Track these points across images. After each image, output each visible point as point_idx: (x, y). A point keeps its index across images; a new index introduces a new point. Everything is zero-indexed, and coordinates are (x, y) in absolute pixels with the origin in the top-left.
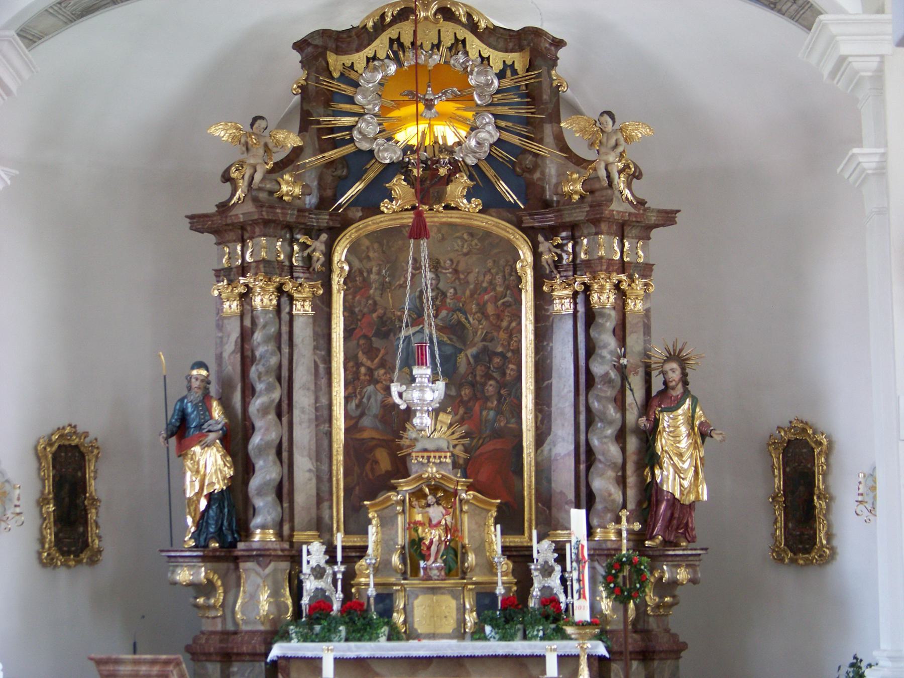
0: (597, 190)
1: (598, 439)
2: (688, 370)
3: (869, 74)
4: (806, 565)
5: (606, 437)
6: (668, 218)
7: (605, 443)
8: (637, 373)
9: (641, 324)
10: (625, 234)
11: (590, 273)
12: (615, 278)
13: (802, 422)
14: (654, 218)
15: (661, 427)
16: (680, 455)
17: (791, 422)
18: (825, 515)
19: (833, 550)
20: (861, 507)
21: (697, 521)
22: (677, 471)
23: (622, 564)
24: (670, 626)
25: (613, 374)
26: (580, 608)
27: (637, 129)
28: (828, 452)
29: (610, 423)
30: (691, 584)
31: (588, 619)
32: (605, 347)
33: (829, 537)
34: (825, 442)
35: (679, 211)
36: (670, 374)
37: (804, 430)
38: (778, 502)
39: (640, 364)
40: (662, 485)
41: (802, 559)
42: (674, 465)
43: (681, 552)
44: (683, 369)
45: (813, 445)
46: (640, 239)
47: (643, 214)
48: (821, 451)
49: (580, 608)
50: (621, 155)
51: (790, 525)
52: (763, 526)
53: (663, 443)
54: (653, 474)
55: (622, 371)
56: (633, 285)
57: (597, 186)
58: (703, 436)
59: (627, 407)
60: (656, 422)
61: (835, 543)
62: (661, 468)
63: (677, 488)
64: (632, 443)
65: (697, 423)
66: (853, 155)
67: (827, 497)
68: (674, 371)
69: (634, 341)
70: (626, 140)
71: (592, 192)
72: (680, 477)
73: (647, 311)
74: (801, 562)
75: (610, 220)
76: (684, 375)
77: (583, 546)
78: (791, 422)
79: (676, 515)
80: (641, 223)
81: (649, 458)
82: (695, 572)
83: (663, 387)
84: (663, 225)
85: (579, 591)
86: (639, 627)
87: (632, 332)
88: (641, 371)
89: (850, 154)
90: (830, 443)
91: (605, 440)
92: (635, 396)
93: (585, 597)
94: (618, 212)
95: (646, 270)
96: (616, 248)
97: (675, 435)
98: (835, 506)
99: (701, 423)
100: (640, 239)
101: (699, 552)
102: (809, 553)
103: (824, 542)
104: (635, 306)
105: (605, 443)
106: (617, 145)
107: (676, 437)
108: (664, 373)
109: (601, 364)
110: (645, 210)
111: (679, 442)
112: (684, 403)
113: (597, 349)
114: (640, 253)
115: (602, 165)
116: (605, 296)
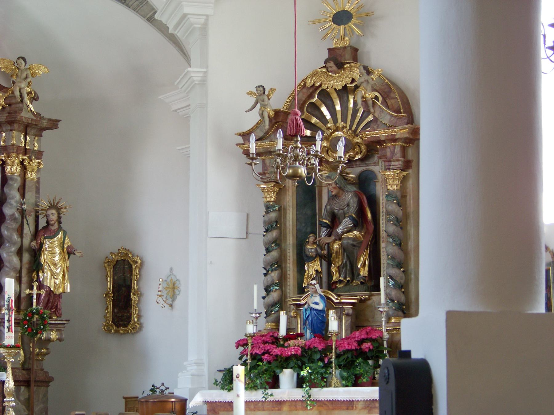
0: (14, 104)
1: (6, 253)
2: (61, 215)
3: (200, 26)
4: (125, 334)
5: (11, 252)
6: (54, 124)
7: (11, 256)
8: (30, 216)
9: (34, 187)
10: (28, 132)
11: (6, 154)
12: (21, 157)
13: (126, 250)
14: (45, 124)
15: (44, 247)
16: (55, 265)
17: (119, 250)
18: (137, 304)
19: (141, 324)
20: (160, 298)
21: (63, 304)
22: (53, 274)
23: (33, 314)
24: (44, 367)
25: (17, 215)
26: (9, 337)
27: (39, 69)
28: (140, 269)
29: (14, 244)
30: (58, 341)
31: (13, 344)
32: (13, 198)
33: (139, 317)
34: (139, 261)
35: (60, 121)
36: (51, 217)
37: (127, 254)
38: (109, 297)
39: (33, 210)
40: (44, 282)
41: (122, 330)
42: (51, 271)
43: (53, 322)
44: (59, 214)
45: (132, 263)
46: (36, 136)
47: (40, 121)
48: (136, 267)
49: (9, 337)
50: (29, 84)
51: (116, 310)
52: (100, 311)
53: (45, 257)
54: (38, 276)
55: (22, 212)
56: (31, 163)
57: (13, 101)
58: (69, 254)
59: (24, 235)
60: (41, 245)
61: (142, 321)
62: (43, 272)
63: (52, 284)
64: (26, 257)
65: (66, 246)
66: (188, 71)
67: (139, 294)
68: (53, 215)
69: (30, 196)
70: (32, 75)
71: (10, 105)
72: (54, 278)
73: (38, 179)
74: (122, 332)
75: (20, 122)
76: (59, 217)
77: (12, 301)
78: (119, 250)
79: (51, 301)
80: (37, 126)
81: (36, 266)
82: (61, 334)
83: (46, 224)
84: (50, 129)
85: (8, 327)
86: (26, 367)
87: (29, 191)
88: (33, 214)
89: (186, 71)
90: (142, 263)
91: (11, 254)
92: (28, 230)
93: (12, 331)
94: (25, 118)
95: (39, 154)
96: (22, 140)
97: (52, 253)
98: (143, 299)
99: (68, 247)
100: (36, 136)
101: (64, 322)
102: (127, 327)
103: (136, 320)
104: (31, 175)
105: (11, 256)
106: (26, 77)
107: (53, 254)
108: (47, 216)
109: (11, 208)
110: (41, 118)
111: (55, 257)
112: (59, 234)
113: (8, 199)
114: (36, 144)
115: (18, 89)
116: (15, 167)
